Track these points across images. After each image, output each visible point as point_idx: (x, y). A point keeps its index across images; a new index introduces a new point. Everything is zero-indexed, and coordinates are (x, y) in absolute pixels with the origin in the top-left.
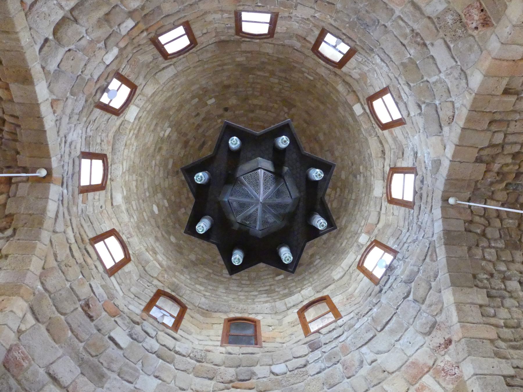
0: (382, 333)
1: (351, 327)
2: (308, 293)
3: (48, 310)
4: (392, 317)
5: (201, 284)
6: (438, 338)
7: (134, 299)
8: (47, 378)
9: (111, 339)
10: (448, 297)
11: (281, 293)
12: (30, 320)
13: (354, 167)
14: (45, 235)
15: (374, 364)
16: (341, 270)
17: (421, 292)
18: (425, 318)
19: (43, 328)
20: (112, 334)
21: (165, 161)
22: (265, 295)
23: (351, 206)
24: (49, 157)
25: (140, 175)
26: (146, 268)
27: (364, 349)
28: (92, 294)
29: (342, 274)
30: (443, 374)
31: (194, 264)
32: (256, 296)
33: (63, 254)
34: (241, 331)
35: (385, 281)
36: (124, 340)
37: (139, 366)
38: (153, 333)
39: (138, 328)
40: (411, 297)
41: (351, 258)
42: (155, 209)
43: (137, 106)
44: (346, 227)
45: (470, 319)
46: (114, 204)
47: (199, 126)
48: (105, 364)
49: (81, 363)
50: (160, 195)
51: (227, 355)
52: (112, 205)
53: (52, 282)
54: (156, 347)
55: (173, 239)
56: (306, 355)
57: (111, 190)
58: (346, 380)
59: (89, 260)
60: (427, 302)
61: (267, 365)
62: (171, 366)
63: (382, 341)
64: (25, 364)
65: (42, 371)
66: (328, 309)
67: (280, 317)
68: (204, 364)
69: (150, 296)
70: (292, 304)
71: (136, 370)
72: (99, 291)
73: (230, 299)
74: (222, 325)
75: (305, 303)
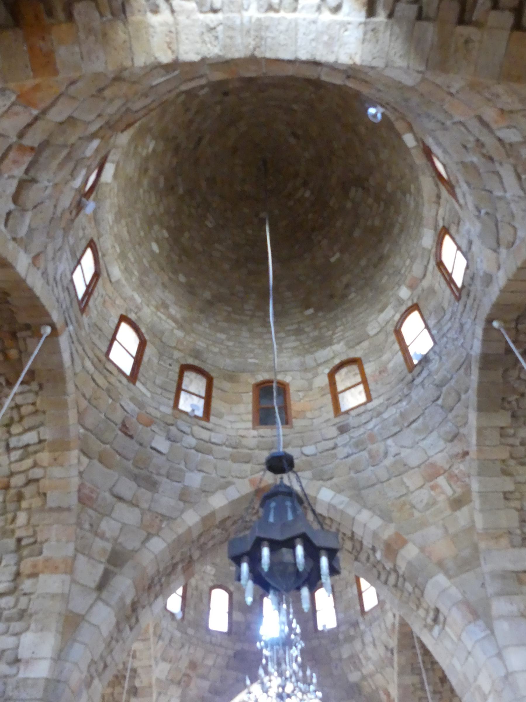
0: (409, 430)
1: (379, 414)
2: (338, 351)
3: (96, 446)
4: (418, 417)
5: (222, 331)
6: (457, 448)
7: (161, 394)
8: (114, 500)
9: (153, 448)
10: (473, 417)
11: (311, 335)
12: (85, 460)
13: (404, 182)
14: (70, 387)
15: (397, 457)
16: (376, 325)
17: (451, 401)
18: (448, 427)
19: (95, 462)
20: (154, 445)
21: (154, 181)
22: (293, 338)
23: (396, 230)
24: (48, 315)
25: (130, 215)
26: (164, 340)
27: (390, 442)
28: (125, 413)
29: (378, 329)
30: (455, 479)
31: (210, 303)
32: (284, 338)
33: (89, 389)
34: (270, 401)
35: (419, 372)
36: (163, 445)
37: (182, 466)
38: (187, 429)
39: (173, 429)
40: (440, 402)
41: (390, 314)
42: (155, 247)
43: (113, 162)
44: (388, 257)
45: (488, 442)
46: (113, 280)
47: (191, 121)
48: (154, 471)
49: (135, 478)
50: (156, 227)
51: (260, 439)
52: (110, 281)
53: (89, 421)
54: (193, 442)
55: (182, 278)
56: (333, 438)
57: (106, 266)
58: (371, 468)
59: (113, 380)
60: (454, 412)
61: (297, 446)
62: (211, 457)
63: (407, 437)
64: (94, 496)
65: (107, 495)
66: (359, 379)
67: (309, 375)
68: (240, 450)
69: (175, 381)
70: (322, 360)
71: (181, 470)
72: (130, 406)
73: (255, 346)
74: (251, 394)
75: (337, 361)
